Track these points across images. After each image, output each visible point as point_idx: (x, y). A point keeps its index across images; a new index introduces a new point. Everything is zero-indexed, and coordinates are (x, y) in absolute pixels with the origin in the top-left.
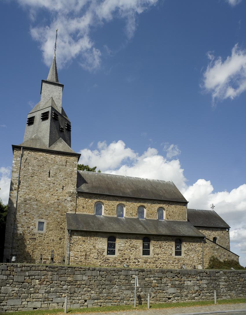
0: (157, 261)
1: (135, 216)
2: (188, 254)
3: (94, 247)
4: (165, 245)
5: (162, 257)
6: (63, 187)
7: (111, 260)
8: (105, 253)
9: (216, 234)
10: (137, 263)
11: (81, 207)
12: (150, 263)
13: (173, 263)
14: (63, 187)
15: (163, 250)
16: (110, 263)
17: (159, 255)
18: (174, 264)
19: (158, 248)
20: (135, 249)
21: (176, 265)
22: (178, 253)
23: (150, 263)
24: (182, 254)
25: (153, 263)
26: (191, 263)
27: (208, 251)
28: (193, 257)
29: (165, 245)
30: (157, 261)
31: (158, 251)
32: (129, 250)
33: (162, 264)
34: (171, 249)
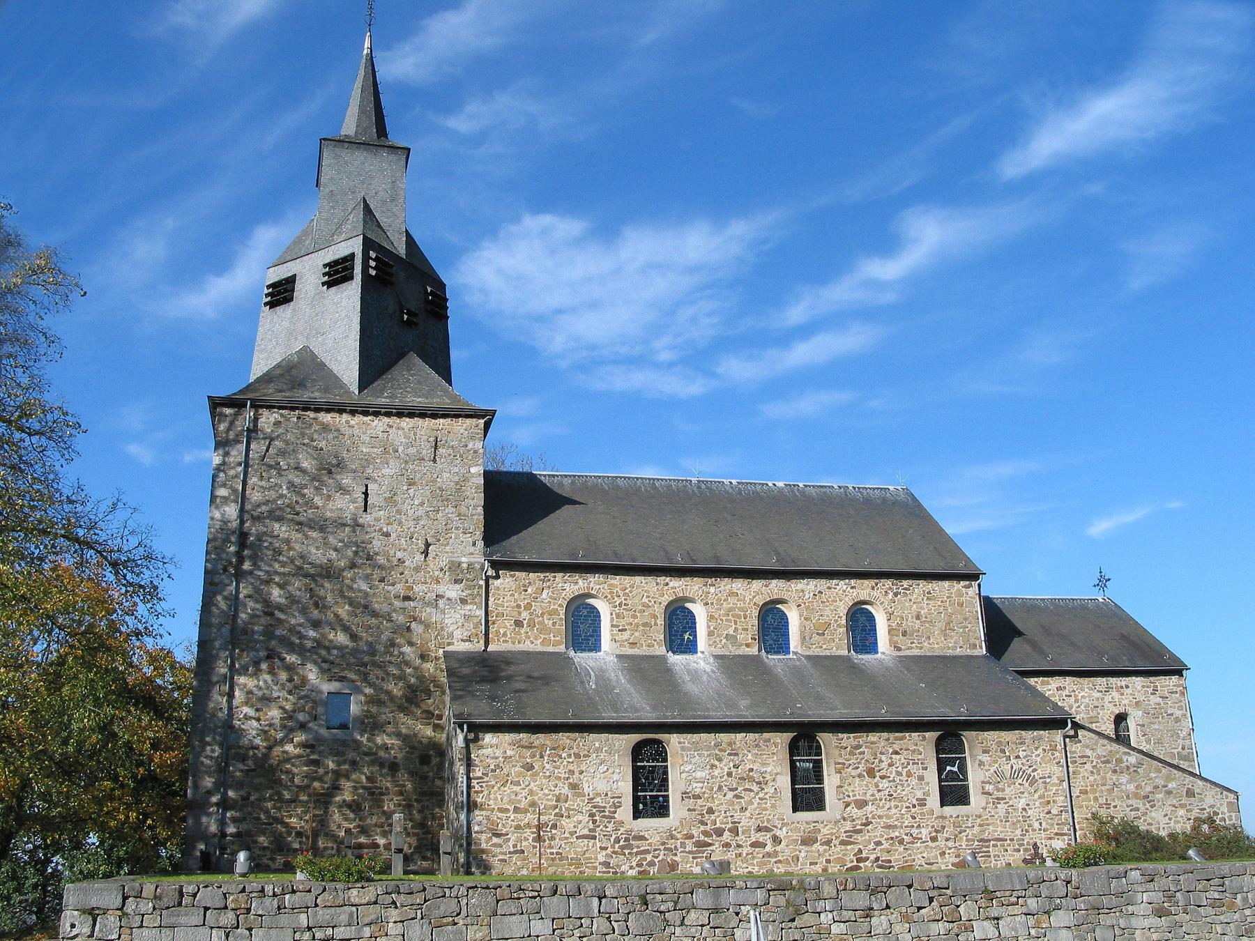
0: (859, 831)
1: (748, 645)
2: (1000, 795)
3: (574, 787)
4: (890, 765)
5: (880, 817)
6: (428, 545)
7: (655, 840)
8: (625, 811)
9: (1126, 702)
10: (769, 848)
11: (509, 624)
12: (828, 843)
13: (934, 839)
14: (428, 545)
15: (884, 784)
16: (647, 852)
17: (869, 808)
18: (941, 843)
19: (860, 776)
20: (755, 788)
21: (950, 844)
22: (954, 794)
23: (828, 843)
24: (972, 799)
25: (843, 843)
26: (1018, 832)
27: (1091, 778)
28: (1024, 809)
29: (890, 765)
30: (859, 831)
31: (859, 788)
32: (730, 795)
33: (886, 845)
34: (921, 778)
